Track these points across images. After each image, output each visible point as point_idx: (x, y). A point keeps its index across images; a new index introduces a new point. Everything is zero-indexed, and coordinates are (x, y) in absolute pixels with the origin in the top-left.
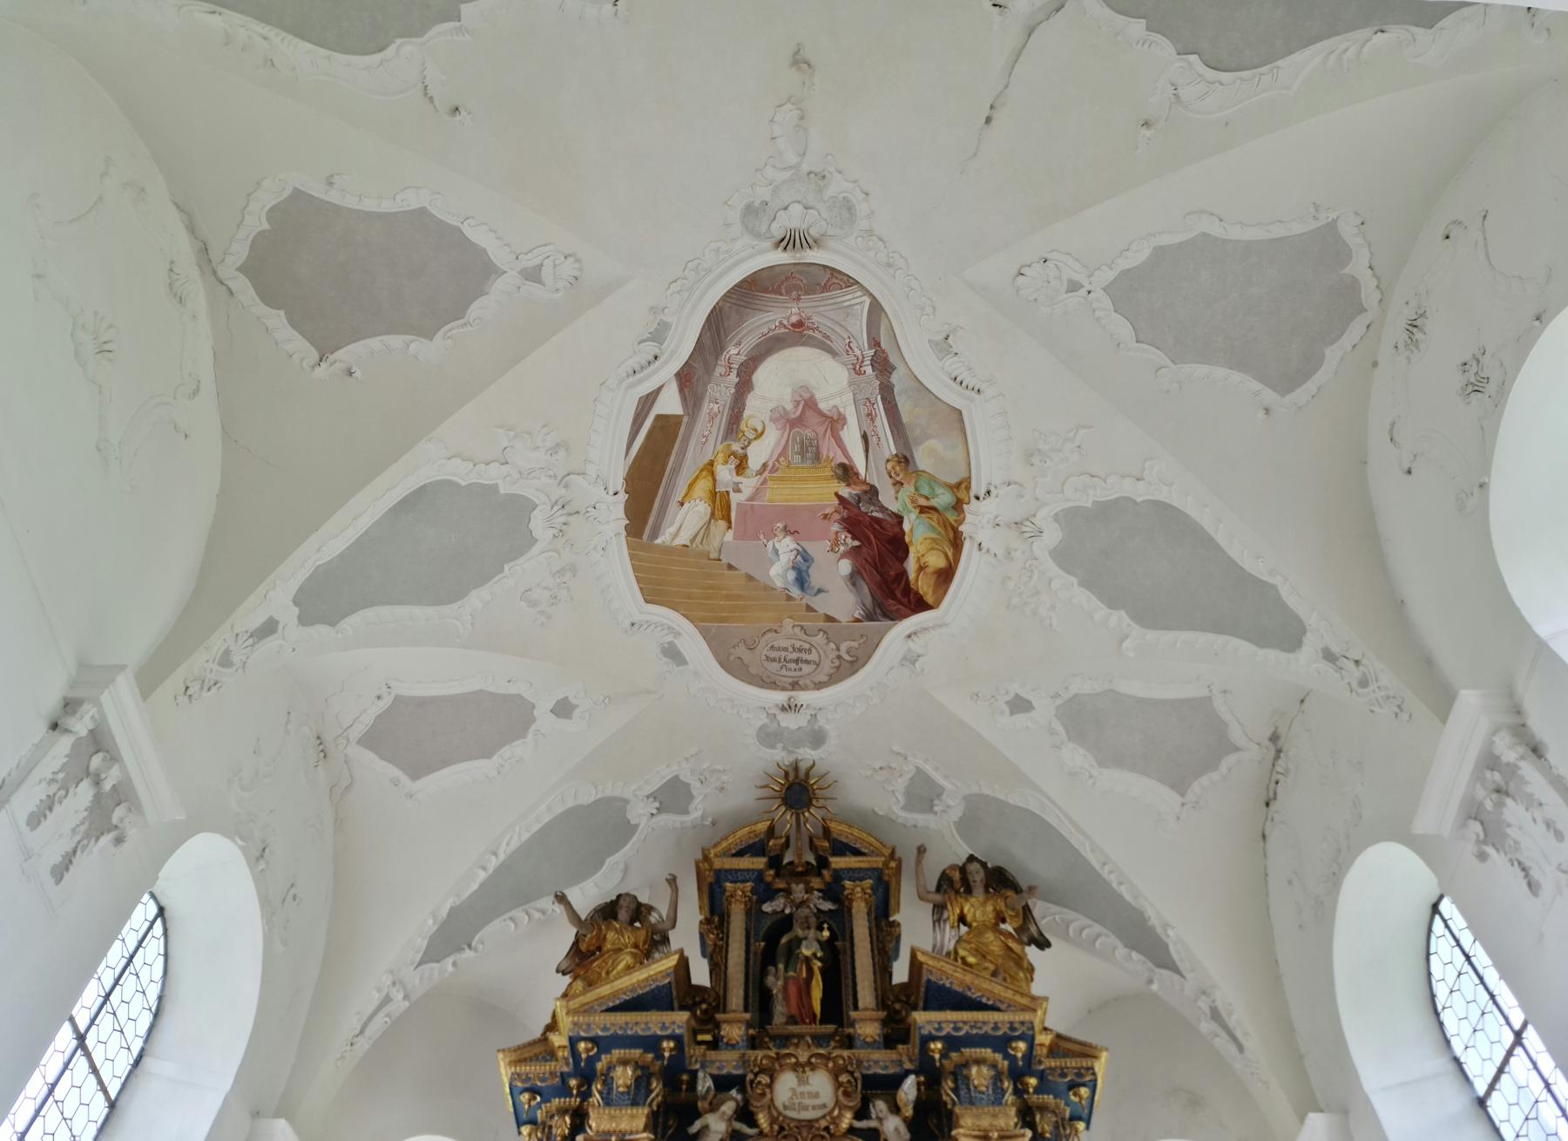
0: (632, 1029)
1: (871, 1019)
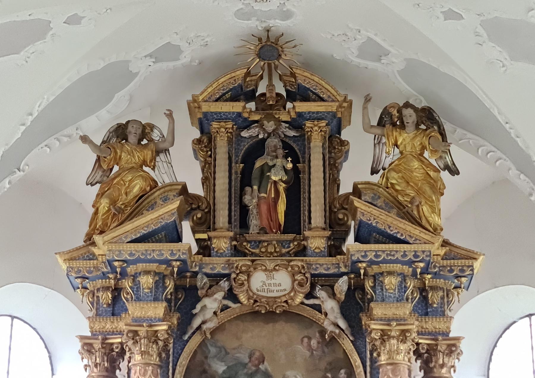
0: (150, 255)
1: (319, 237)
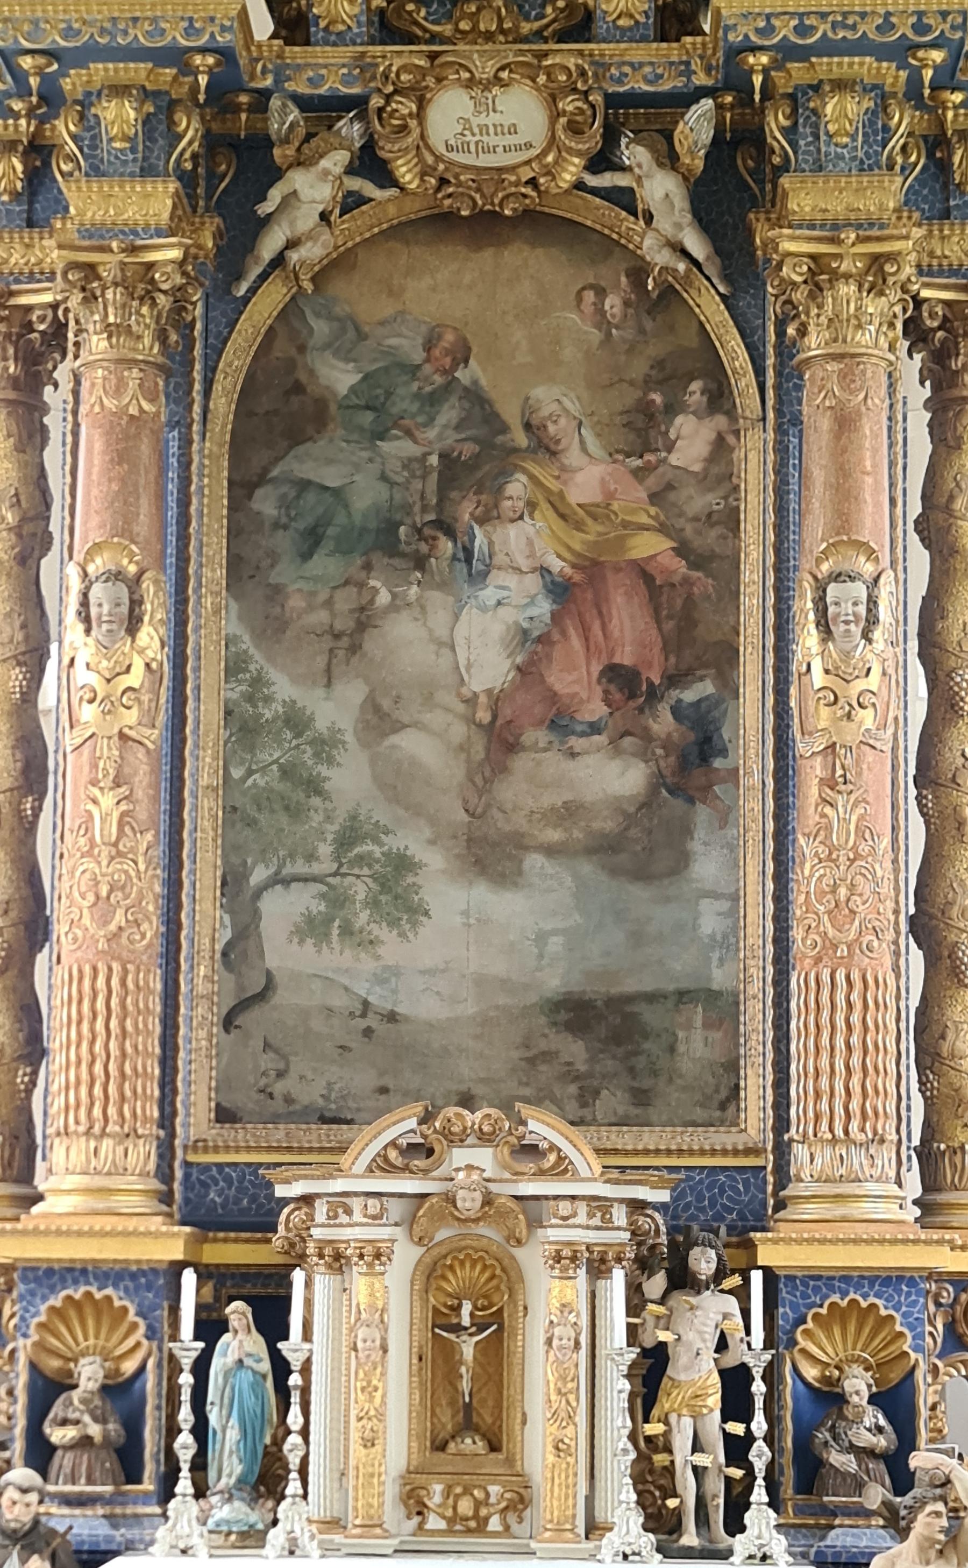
0: (125, 33)
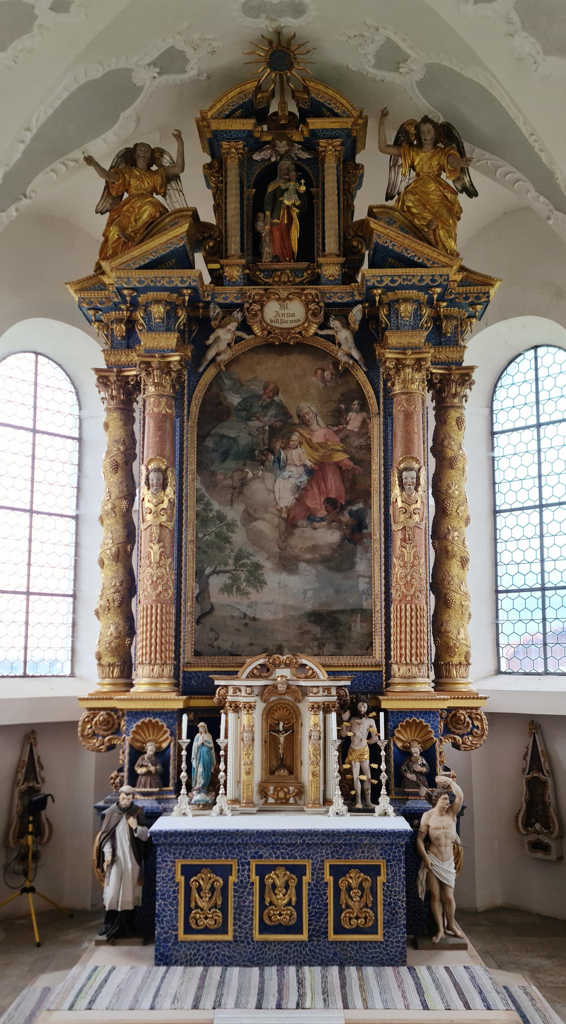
0: (160, 282)
